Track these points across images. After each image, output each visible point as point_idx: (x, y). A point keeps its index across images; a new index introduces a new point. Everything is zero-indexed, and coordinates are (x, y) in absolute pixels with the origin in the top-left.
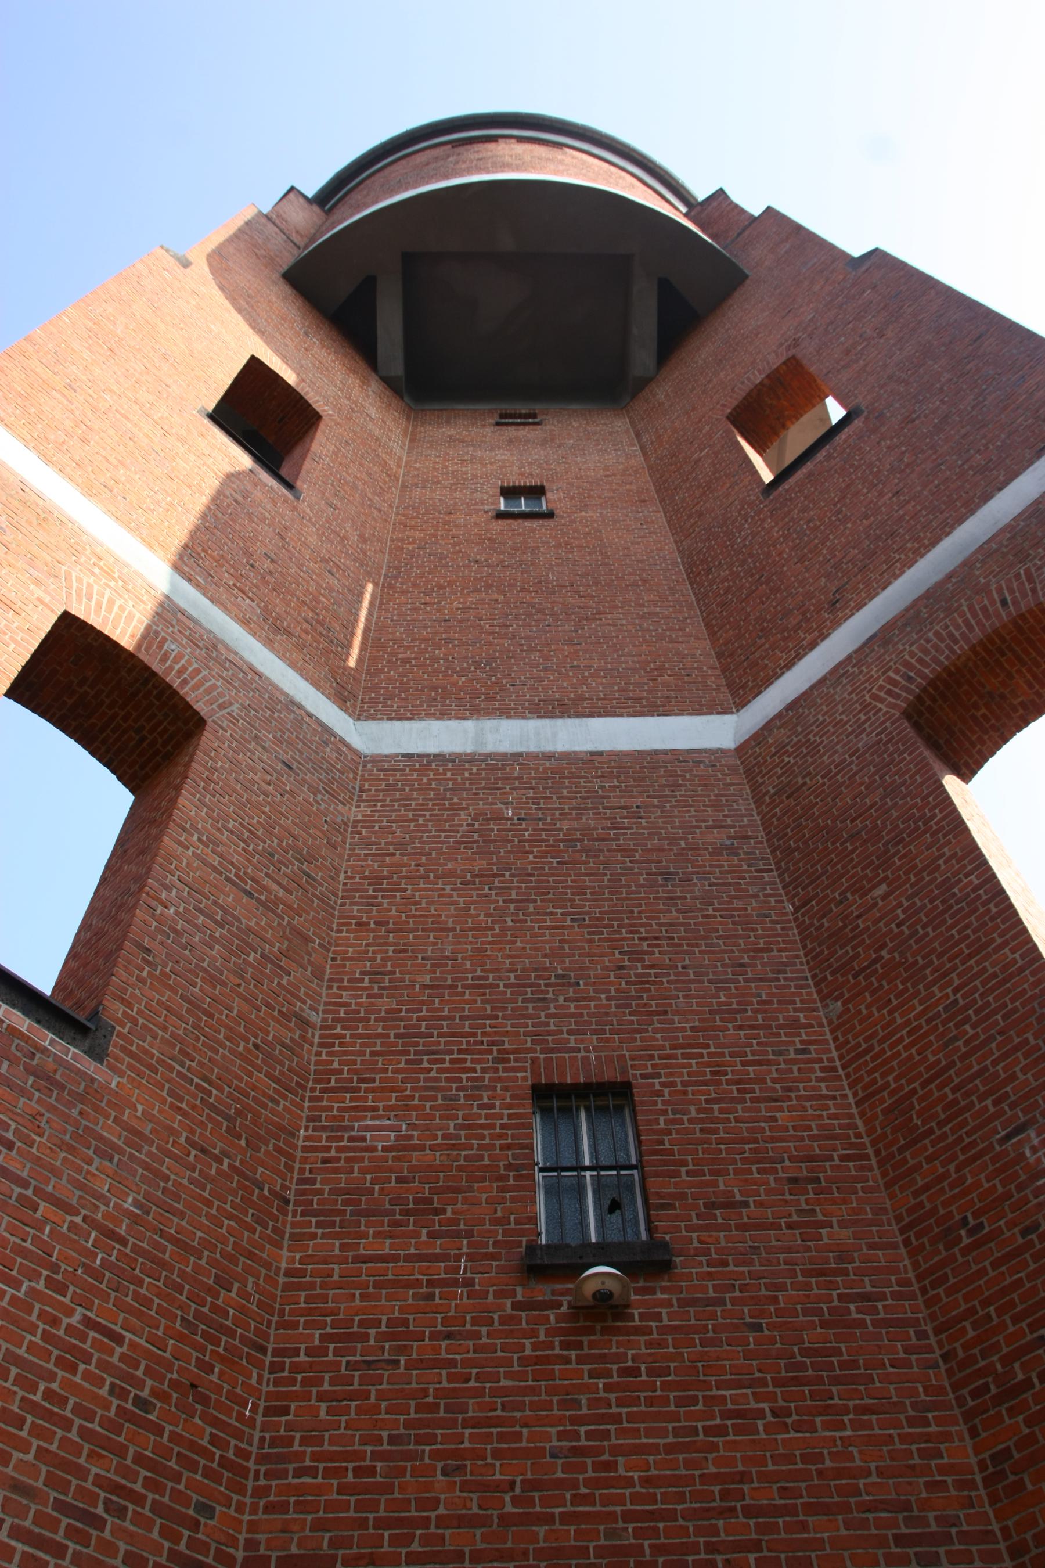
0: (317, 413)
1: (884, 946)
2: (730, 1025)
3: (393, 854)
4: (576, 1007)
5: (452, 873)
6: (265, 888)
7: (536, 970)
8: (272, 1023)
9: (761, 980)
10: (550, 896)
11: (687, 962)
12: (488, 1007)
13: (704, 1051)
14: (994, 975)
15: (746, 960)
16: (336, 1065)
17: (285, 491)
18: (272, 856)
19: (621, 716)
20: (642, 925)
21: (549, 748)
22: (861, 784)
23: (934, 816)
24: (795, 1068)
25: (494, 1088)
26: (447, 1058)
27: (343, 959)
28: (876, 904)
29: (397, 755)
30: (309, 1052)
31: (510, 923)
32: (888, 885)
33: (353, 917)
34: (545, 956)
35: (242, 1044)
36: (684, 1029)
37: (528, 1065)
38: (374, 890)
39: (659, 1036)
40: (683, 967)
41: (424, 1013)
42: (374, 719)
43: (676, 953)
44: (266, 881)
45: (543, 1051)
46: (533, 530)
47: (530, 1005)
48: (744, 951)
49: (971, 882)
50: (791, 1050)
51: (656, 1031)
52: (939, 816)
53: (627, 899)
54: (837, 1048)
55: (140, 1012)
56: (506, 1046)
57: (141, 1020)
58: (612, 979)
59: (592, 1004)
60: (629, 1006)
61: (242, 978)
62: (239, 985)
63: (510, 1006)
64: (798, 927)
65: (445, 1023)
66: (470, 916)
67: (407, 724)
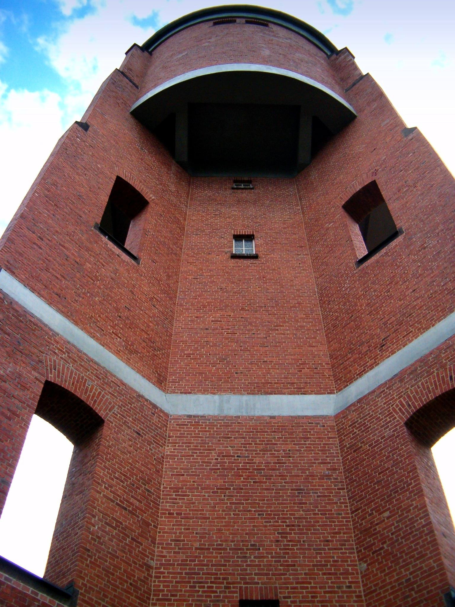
0: (146, 200)
1: (385, 542)
2: (320, 573)
3: (183, 475)
4: (258, 562)
5: (207, 488)
6: (132, 504)
7: (242, 541)
8: (136, 571)
9: (335, 549)
10: (250, 501)
11: (305, 539)
12: (223, 560)
13: (309, 586)
14: (425, 572)
15: (330, 538)
16: (161, 588)
17: (133, 261)
18: (133, 485)
19: (284, 394)
20: (287, 518)
21: (252, 414)
22: (384, 456)
23: (411, 484)
24: (345, 595)
25: (224, 601)
26: (206, 585)
27: (163, 533)
28: (384, 520)
29: (184, 415)
30: (151, 581)
31: (232, 516)
32: (390, 512)
33: (167, 510)
34: (247, 534)
35: (126, 584)
36: (301, 574)
37: (238, 590)
38: (176, 495)
39: (291, 577)
40: (304, 541)
41: (197, 562)
42: (174, 393)
43: (301, 534)
44: (132, 500)
45: (245, 583)
46: (248, 267)
47: (240, 560)
48: (329, 533)
49: (421, 522)
50: (344, 586)
51: (290, 575)
52: (413, 484)
53: (282, 504)
54: (363, 586)
55: (88, 581)
56: (230, 580)
57: (88, 585)
58: (274, 547)
59: (265, 560)
60: (280, 561)
61: (124, 552)
62: (123, 557)
63: (231, 560)
64: (353, 521)
65: (205, 568)
66: (216, 511)
67: (188, 396)
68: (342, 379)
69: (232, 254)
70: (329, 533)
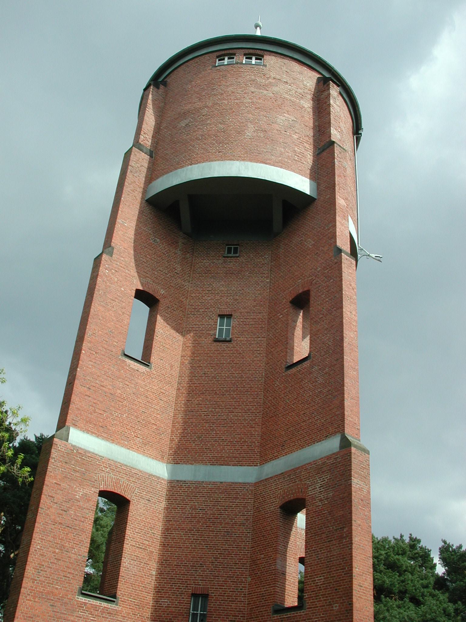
5: (183, 529)
48: (238, 559)
68: (264, 459)
69: (215, 338)
70: (238, 559)
